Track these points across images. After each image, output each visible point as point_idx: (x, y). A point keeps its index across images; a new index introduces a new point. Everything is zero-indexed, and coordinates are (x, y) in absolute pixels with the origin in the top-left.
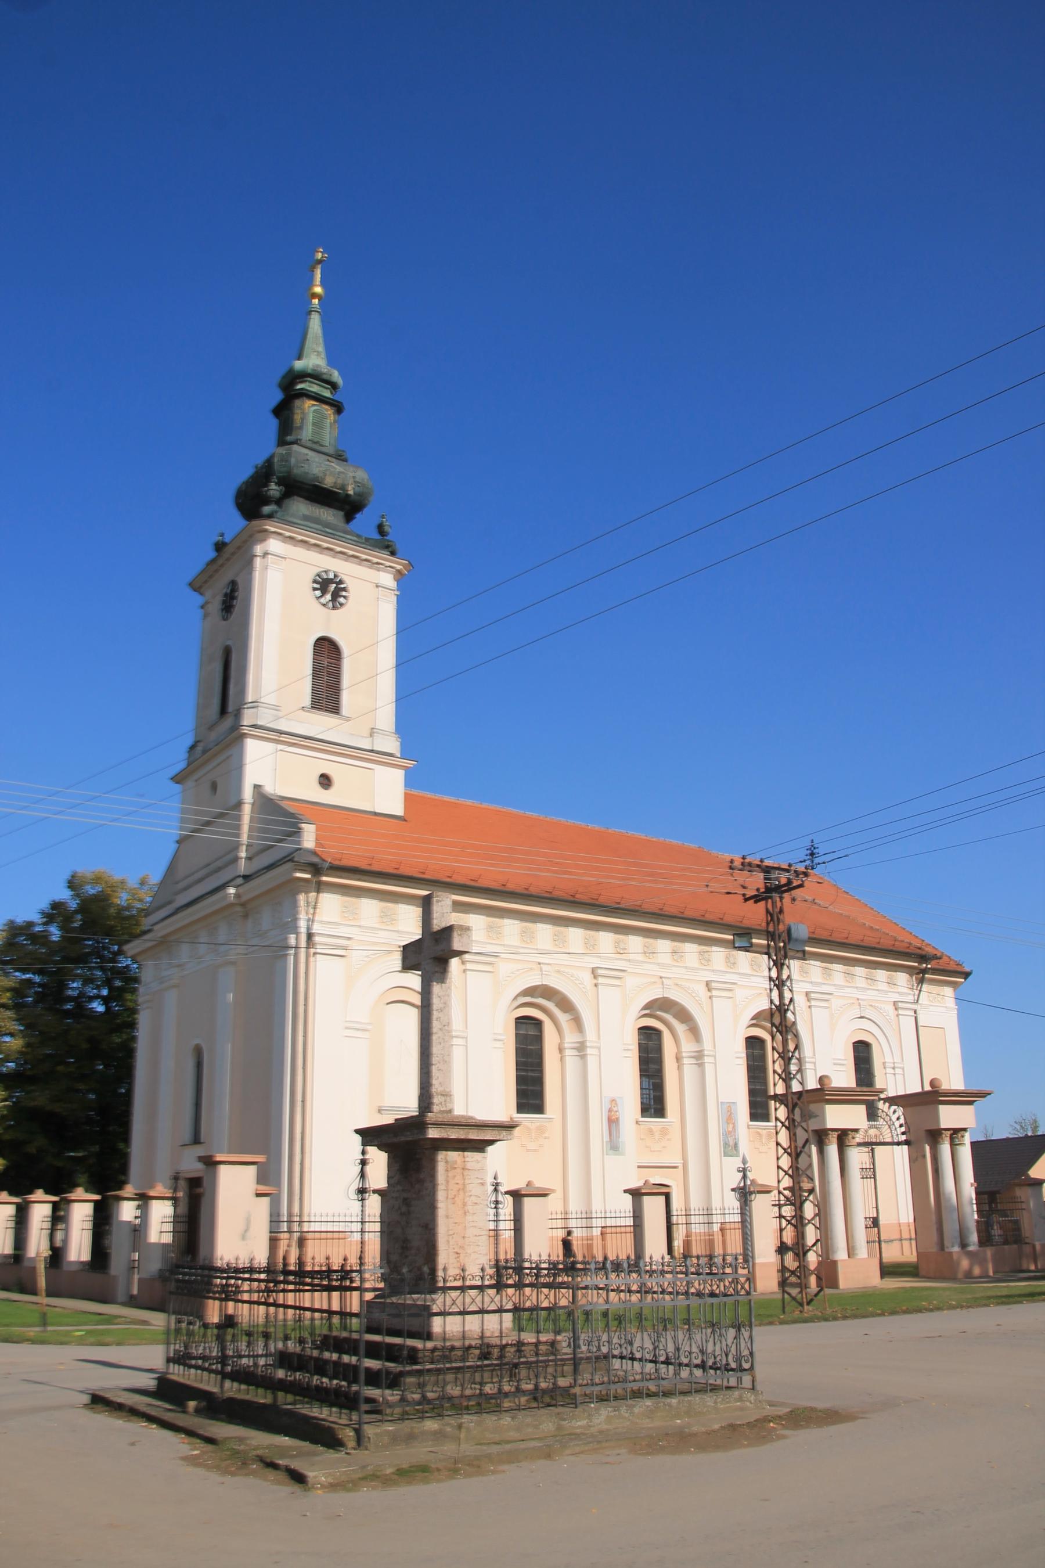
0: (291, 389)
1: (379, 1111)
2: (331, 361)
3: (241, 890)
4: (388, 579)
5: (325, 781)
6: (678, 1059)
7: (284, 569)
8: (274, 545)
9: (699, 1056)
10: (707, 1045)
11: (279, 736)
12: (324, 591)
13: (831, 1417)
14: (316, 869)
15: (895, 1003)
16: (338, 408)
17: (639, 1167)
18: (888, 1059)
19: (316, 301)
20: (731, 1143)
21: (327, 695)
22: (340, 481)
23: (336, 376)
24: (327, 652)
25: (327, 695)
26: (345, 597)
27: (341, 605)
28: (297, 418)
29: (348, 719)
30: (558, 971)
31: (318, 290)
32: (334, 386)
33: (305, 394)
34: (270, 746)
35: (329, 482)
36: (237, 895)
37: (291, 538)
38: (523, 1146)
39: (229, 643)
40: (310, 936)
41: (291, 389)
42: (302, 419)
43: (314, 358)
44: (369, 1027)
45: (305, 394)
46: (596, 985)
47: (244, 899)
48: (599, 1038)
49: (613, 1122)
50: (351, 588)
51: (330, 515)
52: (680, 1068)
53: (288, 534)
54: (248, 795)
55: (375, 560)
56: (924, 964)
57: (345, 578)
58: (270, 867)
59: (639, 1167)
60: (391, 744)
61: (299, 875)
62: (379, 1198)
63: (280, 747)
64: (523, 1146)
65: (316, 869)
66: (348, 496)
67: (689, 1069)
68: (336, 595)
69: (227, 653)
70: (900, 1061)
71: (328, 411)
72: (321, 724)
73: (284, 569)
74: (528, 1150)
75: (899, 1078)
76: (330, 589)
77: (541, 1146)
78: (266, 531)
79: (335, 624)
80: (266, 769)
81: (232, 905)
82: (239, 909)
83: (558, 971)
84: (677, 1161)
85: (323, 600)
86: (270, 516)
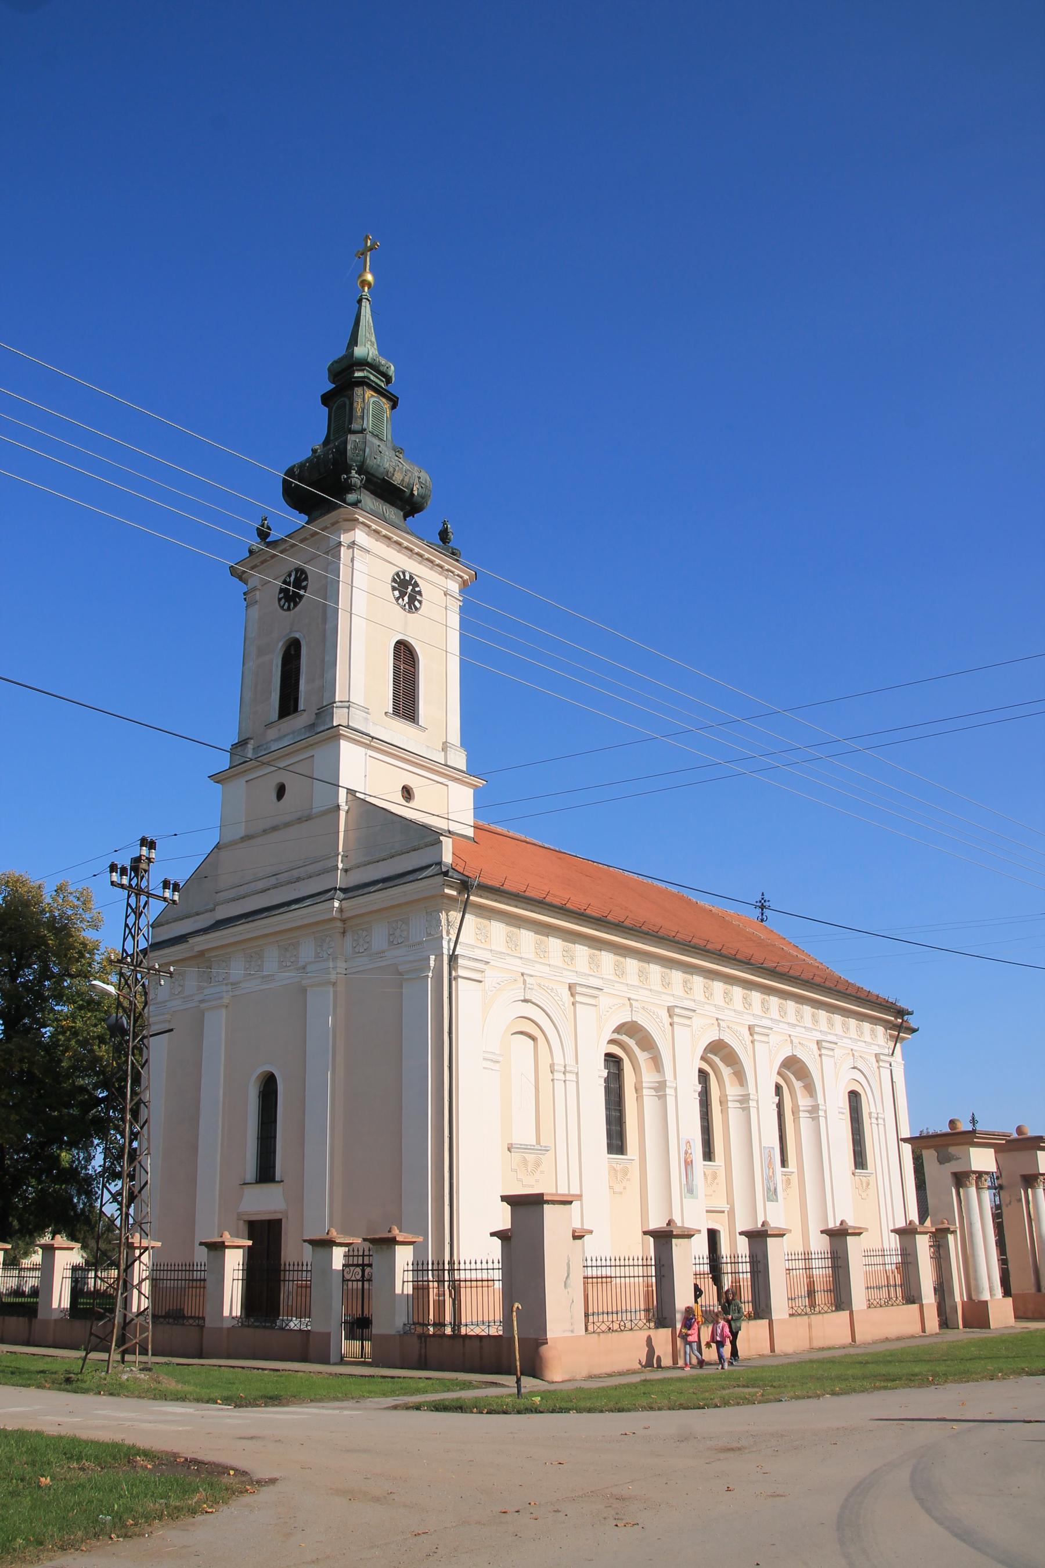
0: (345, 380)
1: (509, 1149)
4: (454, 587)
5: (407, 793)
6: (638, 1089)
7: (369, 559)
8: (360, 536)
9: (814, 1110)
10: (669, 1075)
11: (370, 741)
12: (402, 595)
14: (465, 886)
15: (876, 1055)
16: (394, 403)
17: (708, 1211)
18: (873, 1110)
19: (366, 289)
20: (772, 1189)
21: (406, 704)
22: (407, 479)
23: (392, 371)
24: (405, 655)
25: (406, 704)
27: (416, 609)
28: (358, 407)
30: (643, 1008)
31: (369, 277)
32: (388, 379)
33: (364, 383)
34: (362, 750)
35: (397, 479)
36: (341, 910)
37: (376, 531)
40: (453, 958)
43: (367, 348)
44: (500, 1059)
45: (364, 383)
46: (573, 1004)
47: (346, 915)
48: (577, 1063)
49: (689, 1164)
51: (393, 513)
52: (639, 1098)
55: (447, 567)
56: (897, 1020)
59: (708, 1211)
60: (459, 759)
61: (447, 891)
62: (500, 1241)
63: (370, 753)
65: (465, 886)
66: (412, 494)
67: (650, 1101)
68: (412, 600)
69: (292, 654)
70: (573, 1063)
71: (386, 405)
72: (398, 732)
73: (369, 559)
75: (881, 1127)
76: (406, 588)
77: (537, 1181)
79: (414, 629)
80: (361, 773)
81: (334, 919)
82: (339, 924)
83: (643, 1008)
84: (726, 1207)
86: (355, 504)
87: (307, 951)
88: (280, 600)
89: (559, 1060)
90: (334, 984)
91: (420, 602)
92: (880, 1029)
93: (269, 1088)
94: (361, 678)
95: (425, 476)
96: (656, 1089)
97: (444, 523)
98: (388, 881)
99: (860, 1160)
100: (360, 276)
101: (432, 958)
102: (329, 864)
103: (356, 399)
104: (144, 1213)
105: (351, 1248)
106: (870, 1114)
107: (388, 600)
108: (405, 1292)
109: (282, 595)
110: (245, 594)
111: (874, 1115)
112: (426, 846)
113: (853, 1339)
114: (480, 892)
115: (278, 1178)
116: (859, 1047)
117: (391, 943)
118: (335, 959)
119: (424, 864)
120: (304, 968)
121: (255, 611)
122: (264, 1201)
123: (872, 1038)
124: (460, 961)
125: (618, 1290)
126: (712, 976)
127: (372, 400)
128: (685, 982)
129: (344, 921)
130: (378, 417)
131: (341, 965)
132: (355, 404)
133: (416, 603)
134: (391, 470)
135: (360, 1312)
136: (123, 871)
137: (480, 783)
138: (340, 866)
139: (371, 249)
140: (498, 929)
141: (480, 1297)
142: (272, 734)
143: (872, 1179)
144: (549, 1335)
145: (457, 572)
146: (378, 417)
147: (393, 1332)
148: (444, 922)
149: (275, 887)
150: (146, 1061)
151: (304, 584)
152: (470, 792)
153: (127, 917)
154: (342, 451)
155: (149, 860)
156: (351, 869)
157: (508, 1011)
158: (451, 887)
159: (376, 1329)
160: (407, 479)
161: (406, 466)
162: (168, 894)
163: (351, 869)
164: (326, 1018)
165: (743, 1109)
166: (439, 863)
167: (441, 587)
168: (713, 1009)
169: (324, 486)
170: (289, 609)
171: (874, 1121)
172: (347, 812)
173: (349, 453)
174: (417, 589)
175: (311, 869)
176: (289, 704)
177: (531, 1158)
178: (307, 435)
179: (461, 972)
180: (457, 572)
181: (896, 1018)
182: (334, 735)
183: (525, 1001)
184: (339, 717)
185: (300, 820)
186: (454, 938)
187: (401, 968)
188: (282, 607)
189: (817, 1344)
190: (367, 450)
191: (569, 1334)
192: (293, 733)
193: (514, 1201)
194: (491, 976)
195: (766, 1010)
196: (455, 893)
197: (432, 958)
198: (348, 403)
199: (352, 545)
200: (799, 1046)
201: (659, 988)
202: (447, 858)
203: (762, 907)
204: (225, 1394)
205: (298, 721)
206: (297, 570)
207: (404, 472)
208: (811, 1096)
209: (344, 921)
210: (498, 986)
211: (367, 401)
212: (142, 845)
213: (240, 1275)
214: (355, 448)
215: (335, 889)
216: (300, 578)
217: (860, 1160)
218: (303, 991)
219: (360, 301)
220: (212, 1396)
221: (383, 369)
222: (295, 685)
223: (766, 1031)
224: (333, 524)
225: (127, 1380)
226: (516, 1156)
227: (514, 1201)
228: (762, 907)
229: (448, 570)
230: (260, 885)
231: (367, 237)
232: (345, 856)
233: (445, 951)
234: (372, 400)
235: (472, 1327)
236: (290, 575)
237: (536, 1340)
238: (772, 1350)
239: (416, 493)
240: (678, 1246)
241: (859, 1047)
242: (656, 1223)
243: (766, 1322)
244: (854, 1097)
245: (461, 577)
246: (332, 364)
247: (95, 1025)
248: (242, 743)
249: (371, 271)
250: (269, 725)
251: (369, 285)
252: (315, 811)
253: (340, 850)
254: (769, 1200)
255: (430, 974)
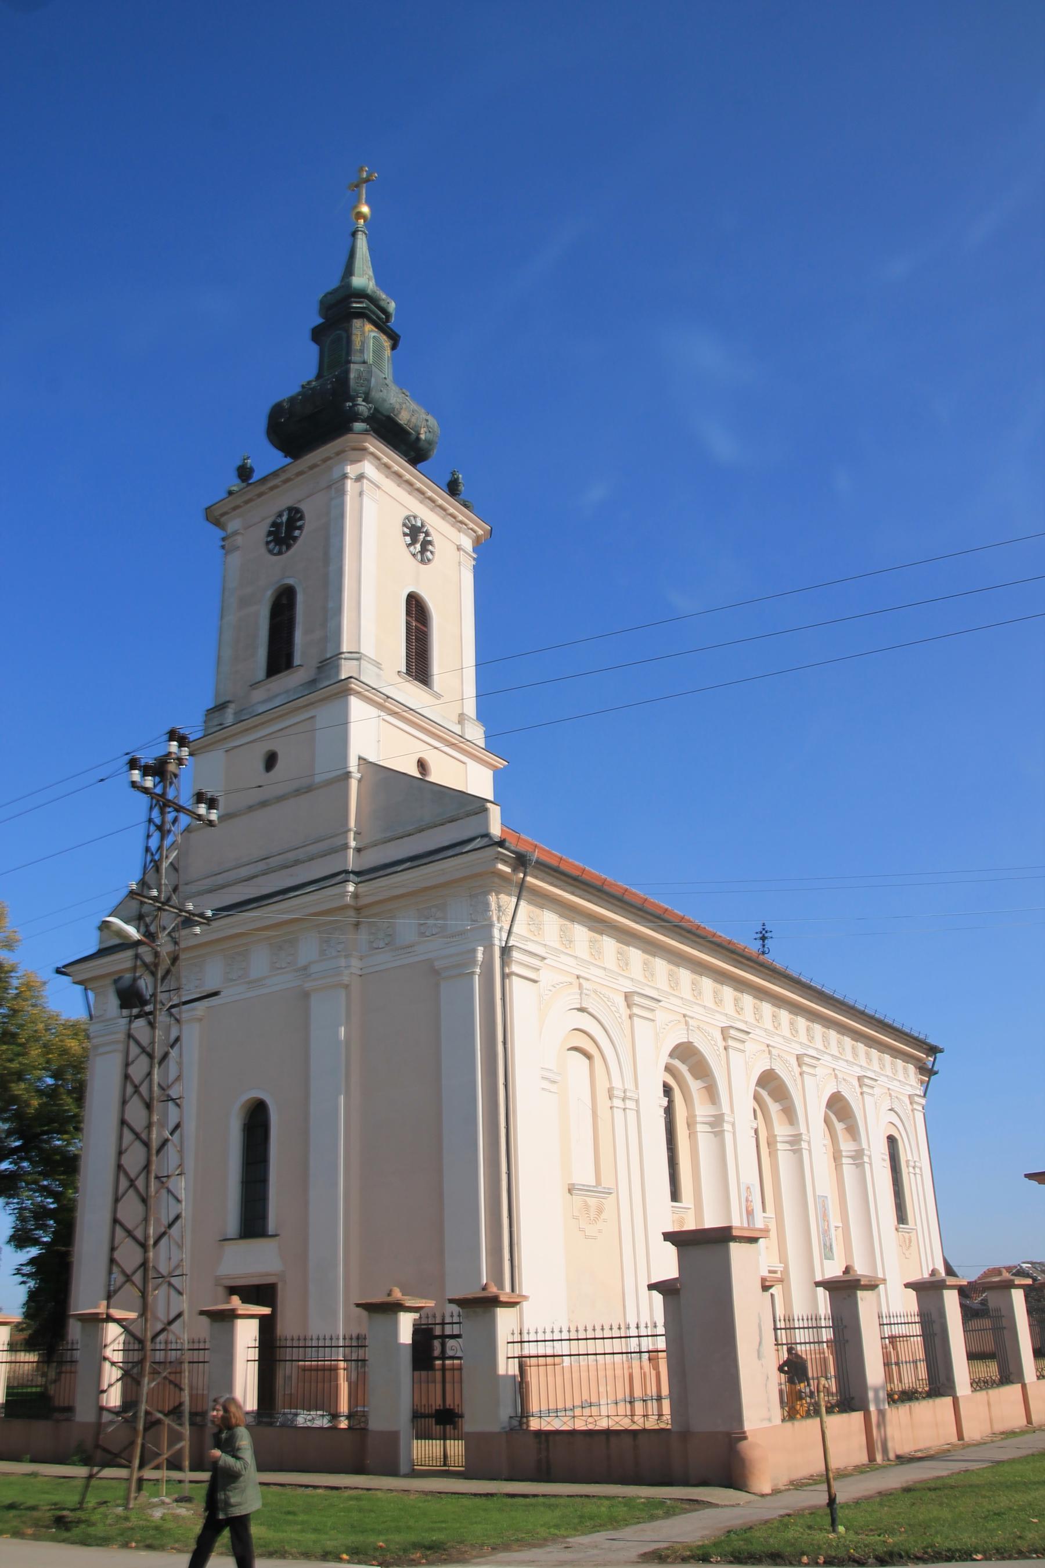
0: (341, 311)
1: (570, 1191)
2: (378, 283)
3: (363, 888)
4: (467, 544)
6: (691, 1124)
8: (368, 467)
11: (385, 704)
12: (414, 541)
13: (717, 1506)
14: (521, 861)
16: (395, 339)
21: (419, 664)
23: (392, 307)
24: (417, 610)
25: (419, 664)
26: (432, 552)
27: (429, 560)
28: (357, 340)
29: (438, 696)
30: (698, 1028)
31: (365, 209)
35: (403, 418)
36: (356, 896)
38: (581, 1230)
39: (290, 581)
40: (506, 951)
41: (341, 311)
42: (363, 343)
43: (363, 279)
44: (557, 1078)
45: (361, 315)
47: (363, 901)
50: (436, 543)
52: (692, 1135)
53: (385, 460)
54: (353, 765)
55: (461, 518)
57: (431, 531)
58: (416, 860)
60: (476, 733)
61: (501, 867)
64: (581, 1230)
65: (521, 861)
66: (418, 439)
69: (283, 607)
70: (633, 1088)
71: (387, 343)
72: (410, 693)
73: (376, 500)
74: (587, 1237)
75: (918, 1176)
77: (600, 1231)
78: (365, 449)
80: (373, 738)
81: (345, 907)
82: (352, 913)
85: (412, 548)
87: (308, 949)
88: (268, 543)
89: (617, 1083)
90: (347, 987)
91: (432, 552)
92: (911, 1068)
93: (256, 1121)
94: (371, 632)
95: (432, 421)
96: (711, 1124)
97: (453, 473)
98: (416, 860)
99: (902, 1217)
100: (355, 207)
101: (481, 949)
102: (338, 841)
103: (354, 331)
104: (174, 1262)
105: (423, 1312)
106: (907, 1161)
107: (395, 546)
108: (511, 1372)
109: (270, 539)
110: (223, 539)
111: (912, 1164)
112: (468, 815)
113: (1029, 1420)
114: (536, 872)
115: (271, 1229)
116: (894, 1085)
117: (422, 934)
118: (347, 956)
119: (465, 838)
120: (305, 968)
121: (235, 560)
122: (254, 1261)
123: (899, 1079)
124: (515, 954)
125: (584, 1375)
126: (762, 996)
127: (373, 334)
128: (736, 1000)
129: (358, 909)
130: (378, 352)
131: (355, 963)
132: (354, 337)
133: (428, 554)
134: (397, 406)
135: (439, 1401)
136: (146, 771)
137: (501, 763)
138: (353, 844)
139: (367, 181)
140: (550, 919)
141: (550, 1379)
142: (258, 695)
143: (913, 1235)
144: (748, 1426)
145: (471, 525)
146: (378, 352)
147: (496, 1429)
148: (493, 906)
149: (264, 873)
150: (177, 1039)
151: (299, 523)
152: (489, 774)
153: (149, 836)
154: (343, 380)
155: (180, 761)
156: (365, 848)
157: (563, 1022)
158: (505, 862)
159: (469, 1425)
160: (413, 420)
161: (413, 406)
162: (202, 809)
163: (365, 848)
164: (335, 1029)
165: (794, 1151)
166: (487, 835)
167: (454, 540)
168: (763, 1033)
169: (317, 422)
170: (280, 553)
171: (911, 1170)
172: (360, 781)
173: (352, 383)
174: (429, 538)
175: (313, 849)
176: (280, 658)
177: (592, 1202)
178: (297, 368)
179: (515, 968)
180: (471, 525)
181: (928, 1055)
182: (343, 690)
183: (582, 1010)
184: (347, 669)
185: (298, 792)
186: (507, 927)
187: (437, 964)
188: (271, 552)
189: (999, 1427)
190: (373, 380)
191: (766, 1424)
192: (287, 692)
193: (681, 1240)
194: (546, 976)
195: (811, 1038)
196: (508, 870)
197: (481, 949)
198: (344, 335)
199: (360, 478)
200: (843, 1082)
201: (712, 1005)
202: (496, 829)
203: (763, 938)
204: (352, 1539)
205: (290, 681)
206: (290, 509)
207: (410, 413)
208: (854, 1140)
209: (358, 909)
210: (553, 989)
211: (366, 336)
212: (171, 739)
213: (254, 1354)
214: (359, 377)
215: (347, 872)
216: (295, 517)
217: (902, 1217)
218: (306, 995)
219: (354, 234)
220: (330, 1545)
221: (383, 304)
222: (289, 639)
223: (814, 1062)
224: (338, 454)
225: (163, 1518)
226: (578, 1199)
227: (681, 1240)
228: (763, 938)
229: (461, 522)
230: (244, 872)
231: (361, 169)
232: (357, 833)
233: (497, 942)
234: (373, 334)
235: (617, 1419)
236: (280, 515)
237: (728, 1434)
238: (960, 1436)
239: (423, 437)
240: (865, 1300)
241: (894, 1085)
242: (834, 1270)
243: (948, 1400)
244: (892, 1140)
245: (475, 532)
246: (325, 296)
247: (11, 1061)
248: (220, 707)
249: (368, 203)
250: (254, 685)
251: (364, 217)
252: (318, 779)
253: (352, 823)
254: (827, 1258)
255: (478, 970)
